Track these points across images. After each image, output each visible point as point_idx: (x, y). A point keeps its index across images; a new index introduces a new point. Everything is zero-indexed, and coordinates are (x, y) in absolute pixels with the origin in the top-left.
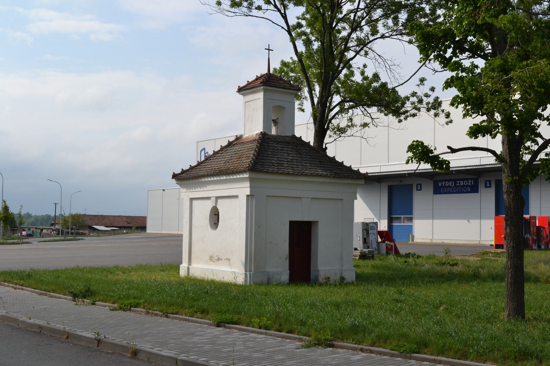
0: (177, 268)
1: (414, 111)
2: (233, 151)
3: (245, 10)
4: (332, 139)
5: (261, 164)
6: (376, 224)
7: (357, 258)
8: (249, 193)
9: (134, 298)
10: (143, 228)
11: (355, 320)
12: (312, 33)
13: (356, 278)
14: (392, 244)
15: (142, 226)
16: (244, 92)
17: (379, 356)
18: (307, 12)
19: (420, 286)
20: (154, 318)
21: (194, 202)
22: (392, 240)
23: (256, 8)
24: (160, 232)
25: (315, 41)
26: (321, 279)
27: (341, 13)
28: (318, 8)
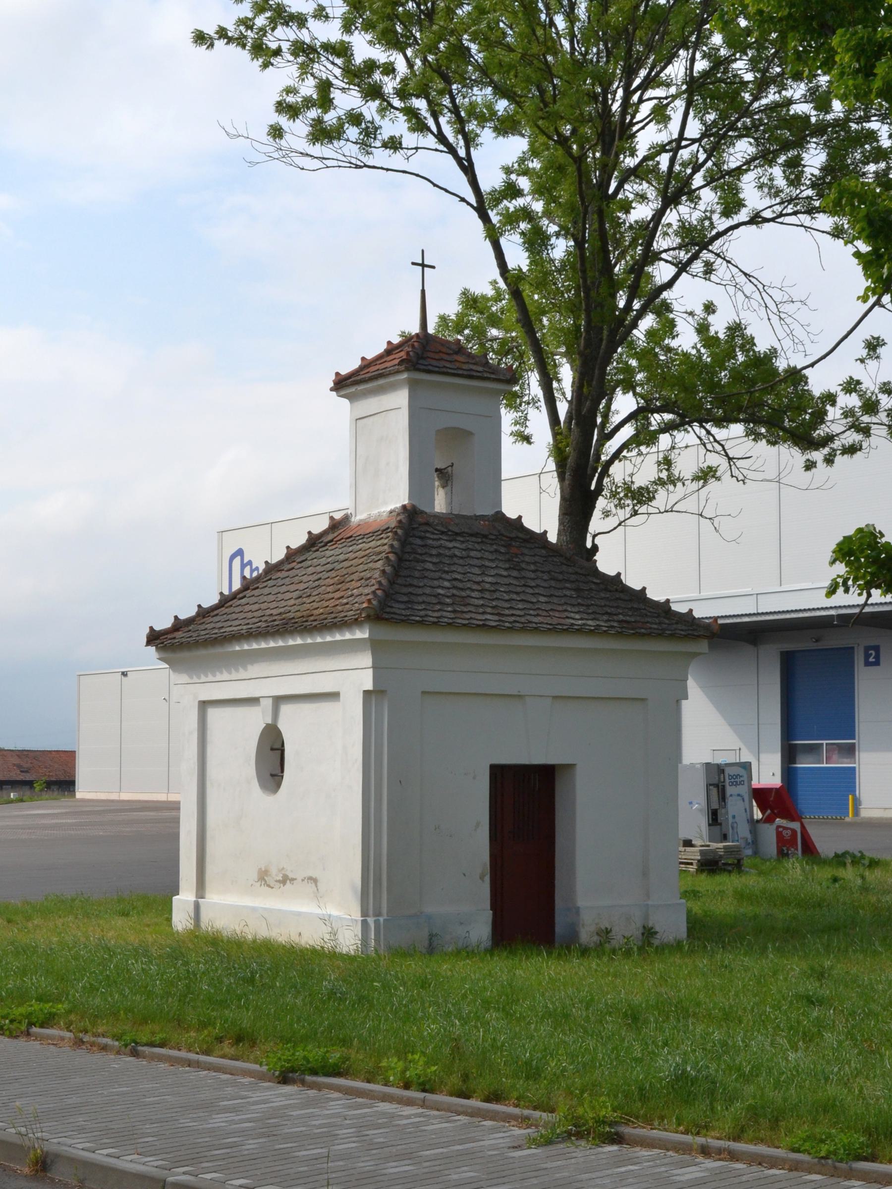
0: (167, 908)
1: (852, 437)
2: (323, 561)
3: (352, 150)
4: (612, 522)
5: (405, 599)
6: (747, 766)
7: (692, 869)
8: (369, 686)
9: (40, 999)
10: (67, 785)
11: (685, 1062)
12: (547, 213)
13: (689, 930)
14: (796, 825)
15: (62, 778)
16: (352, 390)
17: (755, 1168)
18: (534, 152)
19: (876, 953)
20: (98, 1058)
21: (213, 713)
22: (791, 814)
23: (385, 145)
24: (114, 797)
25: (557, 234)
26: (586, 936)
27: (633, 154)
28: (563, 141)
